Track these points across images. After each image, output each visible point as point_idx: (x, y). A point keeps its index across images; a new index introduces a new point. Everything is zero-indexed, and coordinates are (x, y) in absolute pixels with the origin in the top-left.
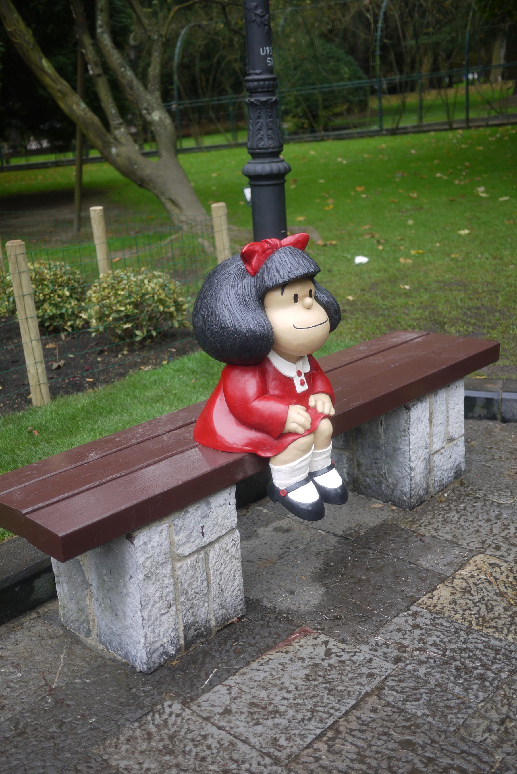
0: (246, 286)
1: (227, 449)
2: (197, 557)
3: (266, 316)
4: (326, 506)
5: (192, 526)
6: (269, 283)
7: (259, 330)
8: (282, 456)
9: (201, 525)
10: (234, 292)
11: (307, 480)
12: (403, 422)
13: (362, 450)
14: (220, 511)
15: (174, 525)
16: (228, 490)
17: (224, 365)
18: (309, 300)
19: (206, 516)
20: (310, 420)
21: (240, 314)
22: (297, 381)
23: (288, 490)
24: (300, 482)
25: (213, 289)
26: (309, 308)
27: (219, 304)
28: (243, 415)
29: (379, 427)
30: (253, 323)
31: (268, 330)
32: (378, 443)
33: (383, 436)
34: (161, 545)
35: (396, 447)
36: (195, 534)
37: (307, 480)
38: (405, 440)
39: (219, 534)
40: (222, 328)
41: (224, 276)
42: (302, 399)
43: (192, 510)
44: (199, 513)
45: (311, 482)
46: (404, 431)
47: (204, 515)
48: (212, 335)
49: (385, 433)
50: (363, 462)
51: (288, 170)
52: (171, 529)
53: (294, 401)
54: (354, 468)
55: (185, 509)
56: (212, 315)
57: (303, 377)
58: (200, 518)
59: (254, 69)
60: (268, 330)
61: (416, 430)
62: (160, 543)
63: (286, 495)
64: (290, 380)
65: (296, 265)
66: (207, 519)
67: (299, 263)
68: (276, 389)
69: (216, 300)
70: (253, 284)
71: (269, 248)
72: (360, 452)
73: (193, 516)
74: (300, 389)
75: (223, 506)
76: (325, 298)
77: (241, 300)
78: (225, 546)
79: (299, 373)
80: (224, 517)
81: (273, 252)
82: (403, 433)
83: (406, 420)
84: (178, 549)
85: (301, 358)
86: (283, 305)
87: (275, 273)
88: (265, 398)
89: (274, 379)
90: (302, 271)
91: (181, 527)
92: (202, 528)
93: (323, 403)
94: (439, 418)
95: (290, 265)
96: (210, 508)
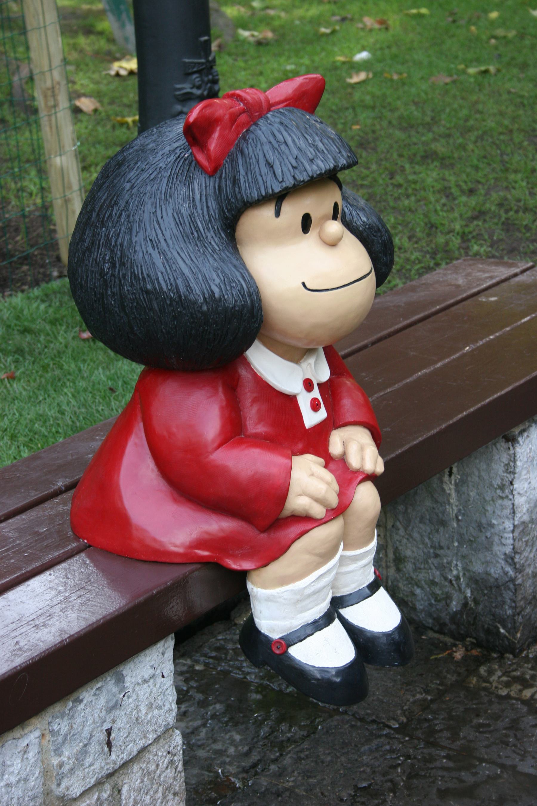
0: (197, 197)
1: (159, 558)
2: (99, 799)
3: (244, 265)
4: (370, 670)
5: (87, 729)
7: (231, 298)
8: (276, 568)
9: (106, 726)
10: (170, 212)
11: (327, 619)
12: (499, 468)
13: (406, 529)
14: (143, 691)
15: (52, 732)
16: (160, 645)
17: (139, 368)
18: (335, 227)
19: (117, 706)
20: (336, 487)
21: (188, 262)
22: (304, 402)
23: (290, 640)
24: (315, 622)
25: (122, 204)
27: (138, 239)
28: (189, 480)
29: (446, 478)
30: (217, 281)
31: (250, 296)
32: (443, 512)
33: (453, 499)
34: (26, 780)
35: (484, 521)
36: (94, 748)
37: (327, 619)
38: (503, 507)
39: (141, 743)
40: (147, 292)
41: (145, 175)
42: (315, 442)
43: (87, 695)
44: (102, 701)
45: (337, 621)
46: (502, 487)
47: (111, 704)
48: (123, 308)
49: (458, 491)
50: (408, 553)
52: (45, 742)
53: (300, 446)
54: (387, 567)
55: (74, 696)
56: (123, 264)
57: (316, 393)
58: (104, 713)
60: (250, 296)
61: (526, 485)
62: (24, 776)
63: (286, 651)
65: (310, 152)
66: (117, 713)
67: (316, 147)
68: (260, 420)
69: (131, 228)
70: (211, 191)
71: (243, 111)
72: (402, 532)
73: (91, 707)
74: (311, 419)
75: (151, 681)
76: (362, 220)
77: (188, 230)
78: (154, 767)
79: (308, 385)
80: (150, 707)
81: (253, 121)
82: (499, 492)
83: (508, 465)
84: (59, 785)
85: (309, 352)
86: (276, 237)
88: (240, 443)
89: (255, 401)
90: (322, 165)
91: (66, 736)
93: (358, 447)
95: (295, 152)
96: (123, 688)
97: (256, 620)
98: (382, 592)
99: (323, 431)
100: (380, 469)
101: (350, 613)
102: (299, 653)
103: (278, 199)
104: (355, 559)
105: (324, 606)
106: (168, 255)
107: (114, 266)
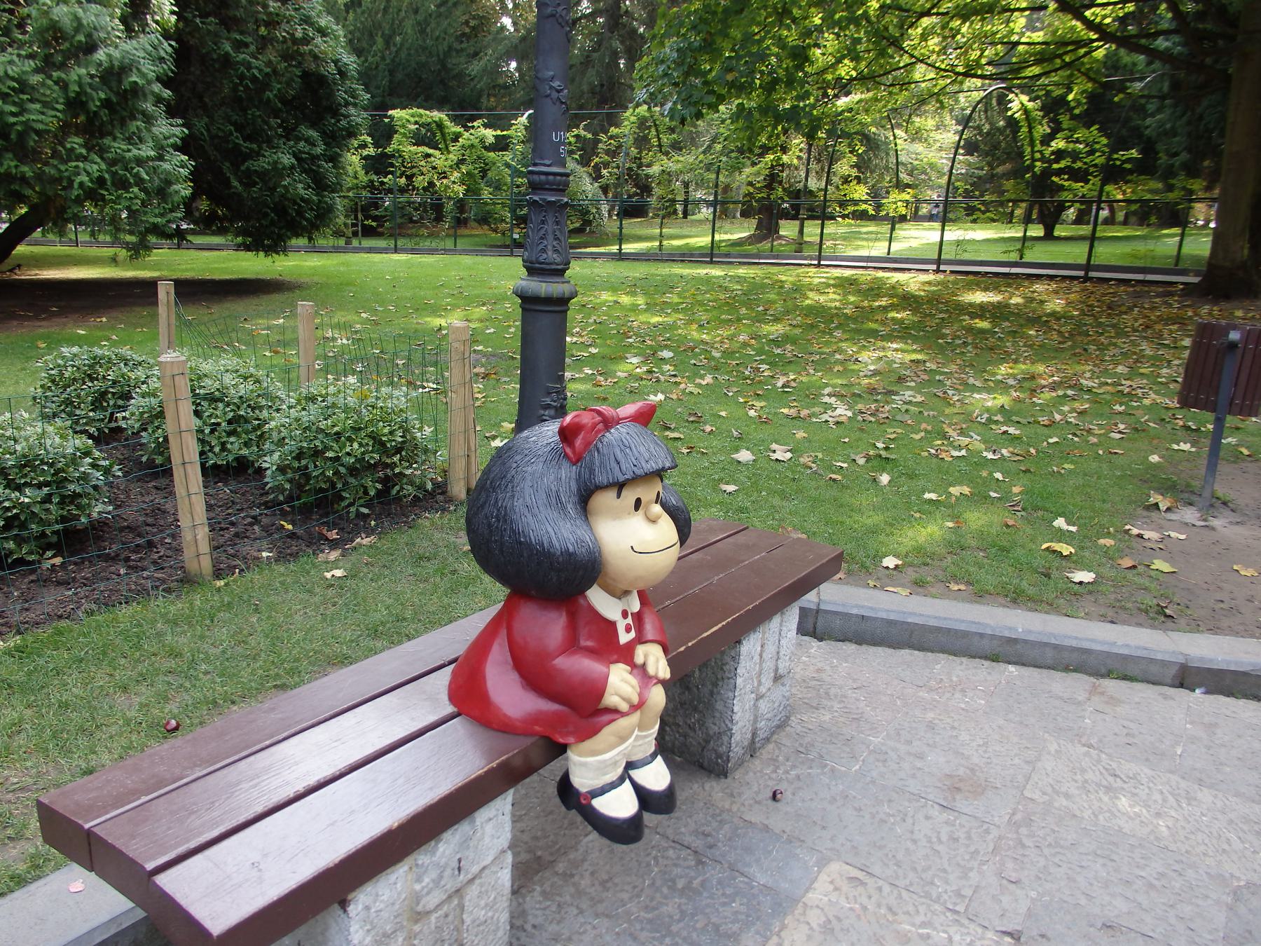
6: (601, 478)
11: (621, 780)
18: (657, 508)
26: (653, 521)
28: (534, 674)
36: (448, 872)
40: (521, 543)
42: (626, 655)
43: (447, 835)
48: (502, 552)
51: (574, 295)
53: (615, 657)
57: (629, 620)
59: (542, 159)
64: (612, 624)
65: (647, 455)
69: (513, 496)
73: (447, 847)
74: (624, 638)
79: (625, 614)
86: (617, 515)
87: (614, 464)
88: (574, 653)
90: (652, 466)
92: (460, 861)
93: (655, 659)
94: (771, 649)
97: (571, 777)
98: (659, 757)
99: (630, 647)
100: (668, 676)
101: (637, 774)
102: (600, 804)
103: (620, 487)
104: (646, 737)
105: (620, 770)
106: (554, 530)
107: (498, 521)
